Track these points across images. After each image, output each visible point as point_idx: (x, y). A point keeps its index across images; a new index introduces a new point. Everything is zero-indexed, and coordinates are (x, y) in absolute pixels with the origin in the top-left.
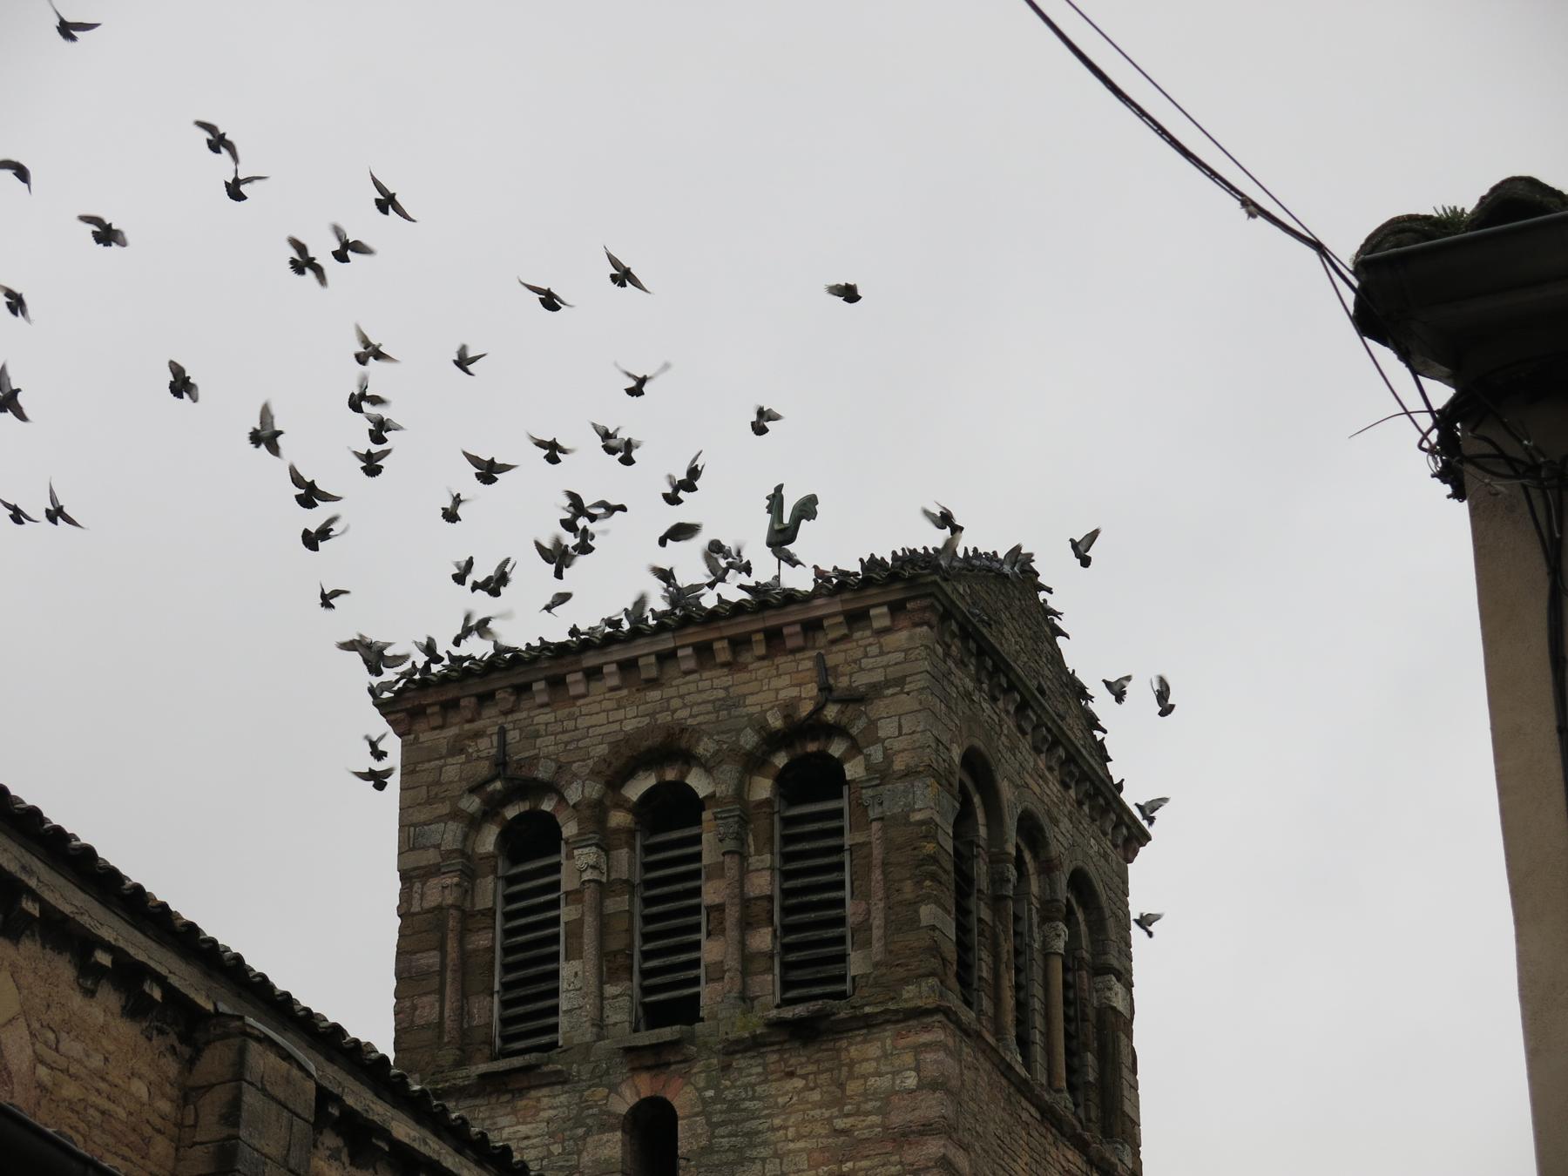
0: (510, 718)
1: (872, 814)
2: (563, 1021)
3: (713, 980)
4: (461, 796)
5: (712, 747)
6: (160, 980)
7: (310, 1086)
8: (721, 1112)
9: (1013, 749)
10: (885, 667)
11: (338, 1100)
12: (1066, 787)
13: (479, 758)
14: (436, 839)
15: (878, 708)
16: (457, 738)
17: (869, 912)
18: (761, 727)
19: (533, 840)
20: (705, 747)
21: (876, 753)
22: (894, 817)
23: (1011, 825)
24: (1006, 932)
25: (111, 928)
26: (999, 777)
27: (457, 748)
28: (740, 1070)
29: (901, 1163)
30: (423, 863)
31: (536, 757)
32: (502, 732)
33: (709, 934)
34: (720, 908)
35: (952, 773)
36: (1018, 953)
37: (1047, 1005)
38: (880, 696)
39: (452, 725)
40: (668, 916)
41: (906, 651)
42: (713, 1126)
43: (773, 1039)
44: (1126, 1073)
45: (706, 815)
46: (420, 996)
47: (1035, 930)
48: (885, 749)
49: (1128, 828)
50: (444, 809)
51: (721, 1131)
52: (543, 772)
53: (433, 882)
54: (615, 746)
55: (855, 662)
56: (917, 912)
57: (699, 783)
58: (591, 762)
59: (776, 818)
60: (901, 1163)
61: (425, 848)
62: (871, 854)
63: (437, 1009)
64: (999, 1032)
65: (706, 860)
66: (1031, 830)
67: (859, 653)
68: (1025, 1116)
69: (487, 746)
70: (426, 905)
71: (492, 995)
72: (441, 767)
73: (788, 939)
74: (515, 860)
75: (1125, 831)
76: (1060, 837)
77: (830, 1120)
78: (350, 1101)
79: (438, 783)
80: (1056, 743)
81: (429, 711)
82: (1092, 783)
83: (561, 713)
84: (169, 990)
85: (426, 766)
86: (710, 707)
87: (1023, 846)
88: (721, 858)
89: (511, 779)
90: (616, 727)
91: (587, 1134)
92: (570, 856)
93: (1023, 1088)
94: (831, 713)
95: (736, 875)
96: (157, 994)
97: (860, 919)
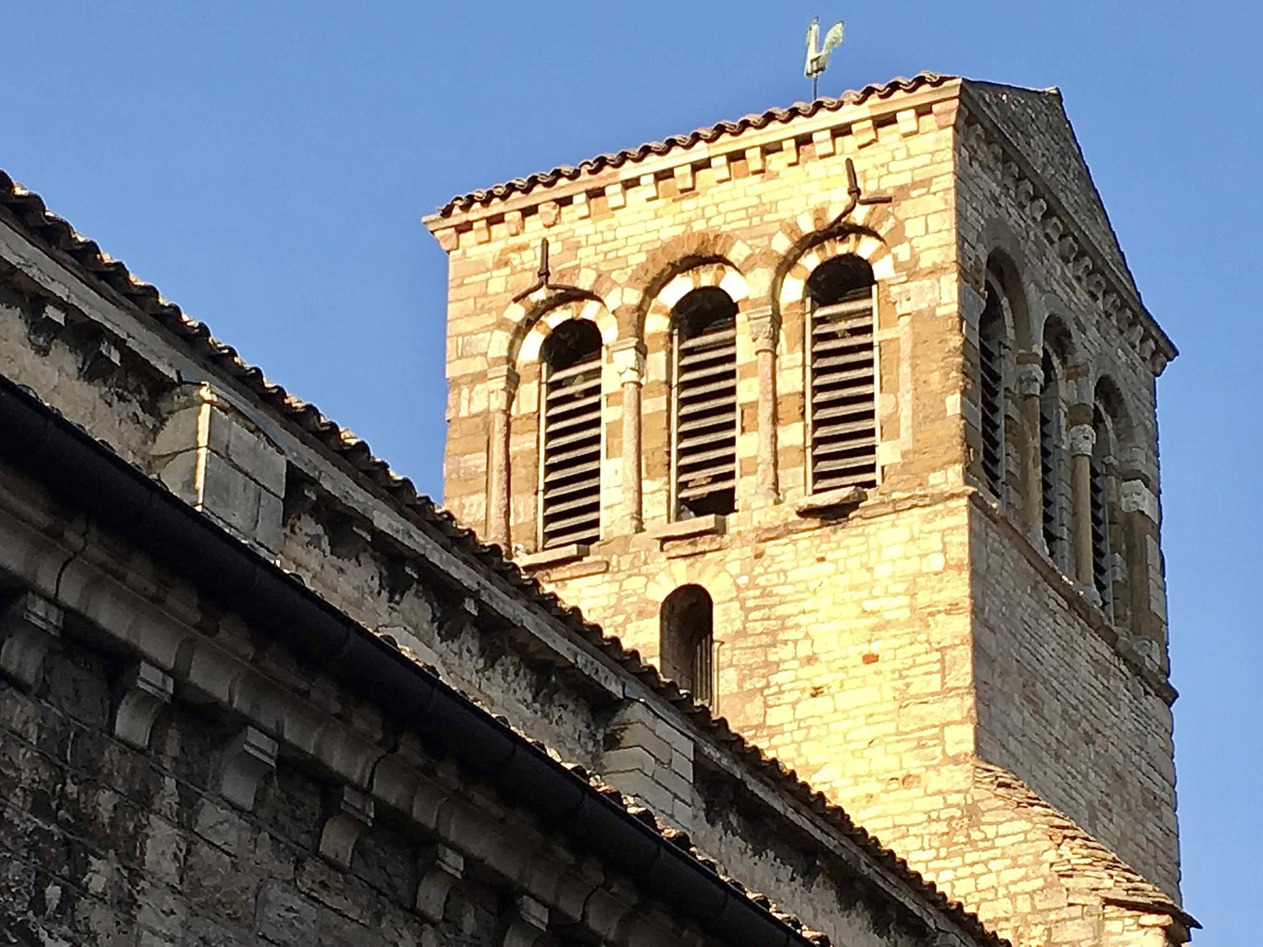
0: (554, 230)
1: (900, 310)
2: (604, 515)
3: (748, 474)
4: (507, 306)
5: (746, 251)
6: (119, 343)
7: (281, 461)
8: (755, 598)
9: (1042, 255)
10: (912, 170)
11: (314, 482)
12: (1094, 297)
13: (524, 270)
14: (482, 347)
15: (905, 208)
16: (503, 252)
17: (897, 405)
18: (791, 229)
19: (574, 345)
20: (737, 253)
21: (903, 252)
22: (920, 313)
23: (1038, 329)
24: (1033, 428)
25: (62, 283)
26: (1025, 279)
27: (503, 262)
28: (773, 557)
29: (927, 641)
30: (471, 371)
31: (578, 267)
32: (545, 244)
33: (743, 430)
34: (754, 405)
35: (978, 271)
36: (1045, 453)
37: (1075, 504)
38: (908, 197)
39: (497, 239)
40: (706, 411)
41: (932, 153)
42: (747, 611)
43: (804, 526)
44: (1153, 574)
45: (740, 318)
46: (468, 495)
47: (1064, 432)
48: (912, 248)
49: (1156, 342)
50: (491, 319)
51: (752, 616)
52: (584, 283)
53: (479, 387)
54: (653, 258)
55: (882, 165)
56: (943, 401)
57: (733, 284)
58: (629, 271)
59: (808, 317)
60: (927, 641)
61: (472, 356)
62: (898, 350)
63: (484, 507)
64: (1023, 514)
65: (740, 360)
66: (1058, 334)
67: (887, 157)
68: (1052, 604)
69: (532, 259)
70: (474, 410)
71: (536, 493)
72: (487, 280)
73: (818, 434)
74: (556, 366)
75: (1152, 343)
76: (1088, 343)
77: (859, 603)
78: (327, 486)
79: (485, 295)
80: (1082, 254)
81: (475, 225)
82: (1120, 296)
83: (602, 225)
84: (129, 356)
85: (475, 279)
86: (743, 214)
87: (1050, 351)
88: (755, 358)
89: (554, 288)
90: (654, 236)
91: (628, 620)
92: (610, 360)
93: (1050, 577)
94: (860, 216)
95: (770, 370)
96: (115, 358)
97: (890, 411)
